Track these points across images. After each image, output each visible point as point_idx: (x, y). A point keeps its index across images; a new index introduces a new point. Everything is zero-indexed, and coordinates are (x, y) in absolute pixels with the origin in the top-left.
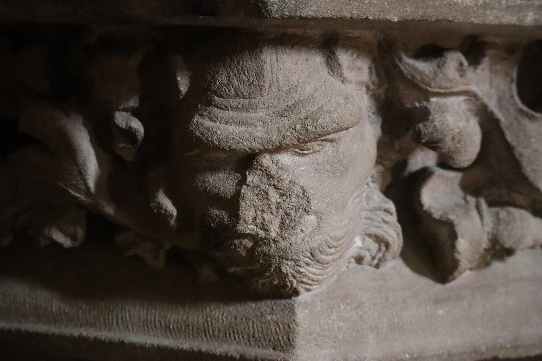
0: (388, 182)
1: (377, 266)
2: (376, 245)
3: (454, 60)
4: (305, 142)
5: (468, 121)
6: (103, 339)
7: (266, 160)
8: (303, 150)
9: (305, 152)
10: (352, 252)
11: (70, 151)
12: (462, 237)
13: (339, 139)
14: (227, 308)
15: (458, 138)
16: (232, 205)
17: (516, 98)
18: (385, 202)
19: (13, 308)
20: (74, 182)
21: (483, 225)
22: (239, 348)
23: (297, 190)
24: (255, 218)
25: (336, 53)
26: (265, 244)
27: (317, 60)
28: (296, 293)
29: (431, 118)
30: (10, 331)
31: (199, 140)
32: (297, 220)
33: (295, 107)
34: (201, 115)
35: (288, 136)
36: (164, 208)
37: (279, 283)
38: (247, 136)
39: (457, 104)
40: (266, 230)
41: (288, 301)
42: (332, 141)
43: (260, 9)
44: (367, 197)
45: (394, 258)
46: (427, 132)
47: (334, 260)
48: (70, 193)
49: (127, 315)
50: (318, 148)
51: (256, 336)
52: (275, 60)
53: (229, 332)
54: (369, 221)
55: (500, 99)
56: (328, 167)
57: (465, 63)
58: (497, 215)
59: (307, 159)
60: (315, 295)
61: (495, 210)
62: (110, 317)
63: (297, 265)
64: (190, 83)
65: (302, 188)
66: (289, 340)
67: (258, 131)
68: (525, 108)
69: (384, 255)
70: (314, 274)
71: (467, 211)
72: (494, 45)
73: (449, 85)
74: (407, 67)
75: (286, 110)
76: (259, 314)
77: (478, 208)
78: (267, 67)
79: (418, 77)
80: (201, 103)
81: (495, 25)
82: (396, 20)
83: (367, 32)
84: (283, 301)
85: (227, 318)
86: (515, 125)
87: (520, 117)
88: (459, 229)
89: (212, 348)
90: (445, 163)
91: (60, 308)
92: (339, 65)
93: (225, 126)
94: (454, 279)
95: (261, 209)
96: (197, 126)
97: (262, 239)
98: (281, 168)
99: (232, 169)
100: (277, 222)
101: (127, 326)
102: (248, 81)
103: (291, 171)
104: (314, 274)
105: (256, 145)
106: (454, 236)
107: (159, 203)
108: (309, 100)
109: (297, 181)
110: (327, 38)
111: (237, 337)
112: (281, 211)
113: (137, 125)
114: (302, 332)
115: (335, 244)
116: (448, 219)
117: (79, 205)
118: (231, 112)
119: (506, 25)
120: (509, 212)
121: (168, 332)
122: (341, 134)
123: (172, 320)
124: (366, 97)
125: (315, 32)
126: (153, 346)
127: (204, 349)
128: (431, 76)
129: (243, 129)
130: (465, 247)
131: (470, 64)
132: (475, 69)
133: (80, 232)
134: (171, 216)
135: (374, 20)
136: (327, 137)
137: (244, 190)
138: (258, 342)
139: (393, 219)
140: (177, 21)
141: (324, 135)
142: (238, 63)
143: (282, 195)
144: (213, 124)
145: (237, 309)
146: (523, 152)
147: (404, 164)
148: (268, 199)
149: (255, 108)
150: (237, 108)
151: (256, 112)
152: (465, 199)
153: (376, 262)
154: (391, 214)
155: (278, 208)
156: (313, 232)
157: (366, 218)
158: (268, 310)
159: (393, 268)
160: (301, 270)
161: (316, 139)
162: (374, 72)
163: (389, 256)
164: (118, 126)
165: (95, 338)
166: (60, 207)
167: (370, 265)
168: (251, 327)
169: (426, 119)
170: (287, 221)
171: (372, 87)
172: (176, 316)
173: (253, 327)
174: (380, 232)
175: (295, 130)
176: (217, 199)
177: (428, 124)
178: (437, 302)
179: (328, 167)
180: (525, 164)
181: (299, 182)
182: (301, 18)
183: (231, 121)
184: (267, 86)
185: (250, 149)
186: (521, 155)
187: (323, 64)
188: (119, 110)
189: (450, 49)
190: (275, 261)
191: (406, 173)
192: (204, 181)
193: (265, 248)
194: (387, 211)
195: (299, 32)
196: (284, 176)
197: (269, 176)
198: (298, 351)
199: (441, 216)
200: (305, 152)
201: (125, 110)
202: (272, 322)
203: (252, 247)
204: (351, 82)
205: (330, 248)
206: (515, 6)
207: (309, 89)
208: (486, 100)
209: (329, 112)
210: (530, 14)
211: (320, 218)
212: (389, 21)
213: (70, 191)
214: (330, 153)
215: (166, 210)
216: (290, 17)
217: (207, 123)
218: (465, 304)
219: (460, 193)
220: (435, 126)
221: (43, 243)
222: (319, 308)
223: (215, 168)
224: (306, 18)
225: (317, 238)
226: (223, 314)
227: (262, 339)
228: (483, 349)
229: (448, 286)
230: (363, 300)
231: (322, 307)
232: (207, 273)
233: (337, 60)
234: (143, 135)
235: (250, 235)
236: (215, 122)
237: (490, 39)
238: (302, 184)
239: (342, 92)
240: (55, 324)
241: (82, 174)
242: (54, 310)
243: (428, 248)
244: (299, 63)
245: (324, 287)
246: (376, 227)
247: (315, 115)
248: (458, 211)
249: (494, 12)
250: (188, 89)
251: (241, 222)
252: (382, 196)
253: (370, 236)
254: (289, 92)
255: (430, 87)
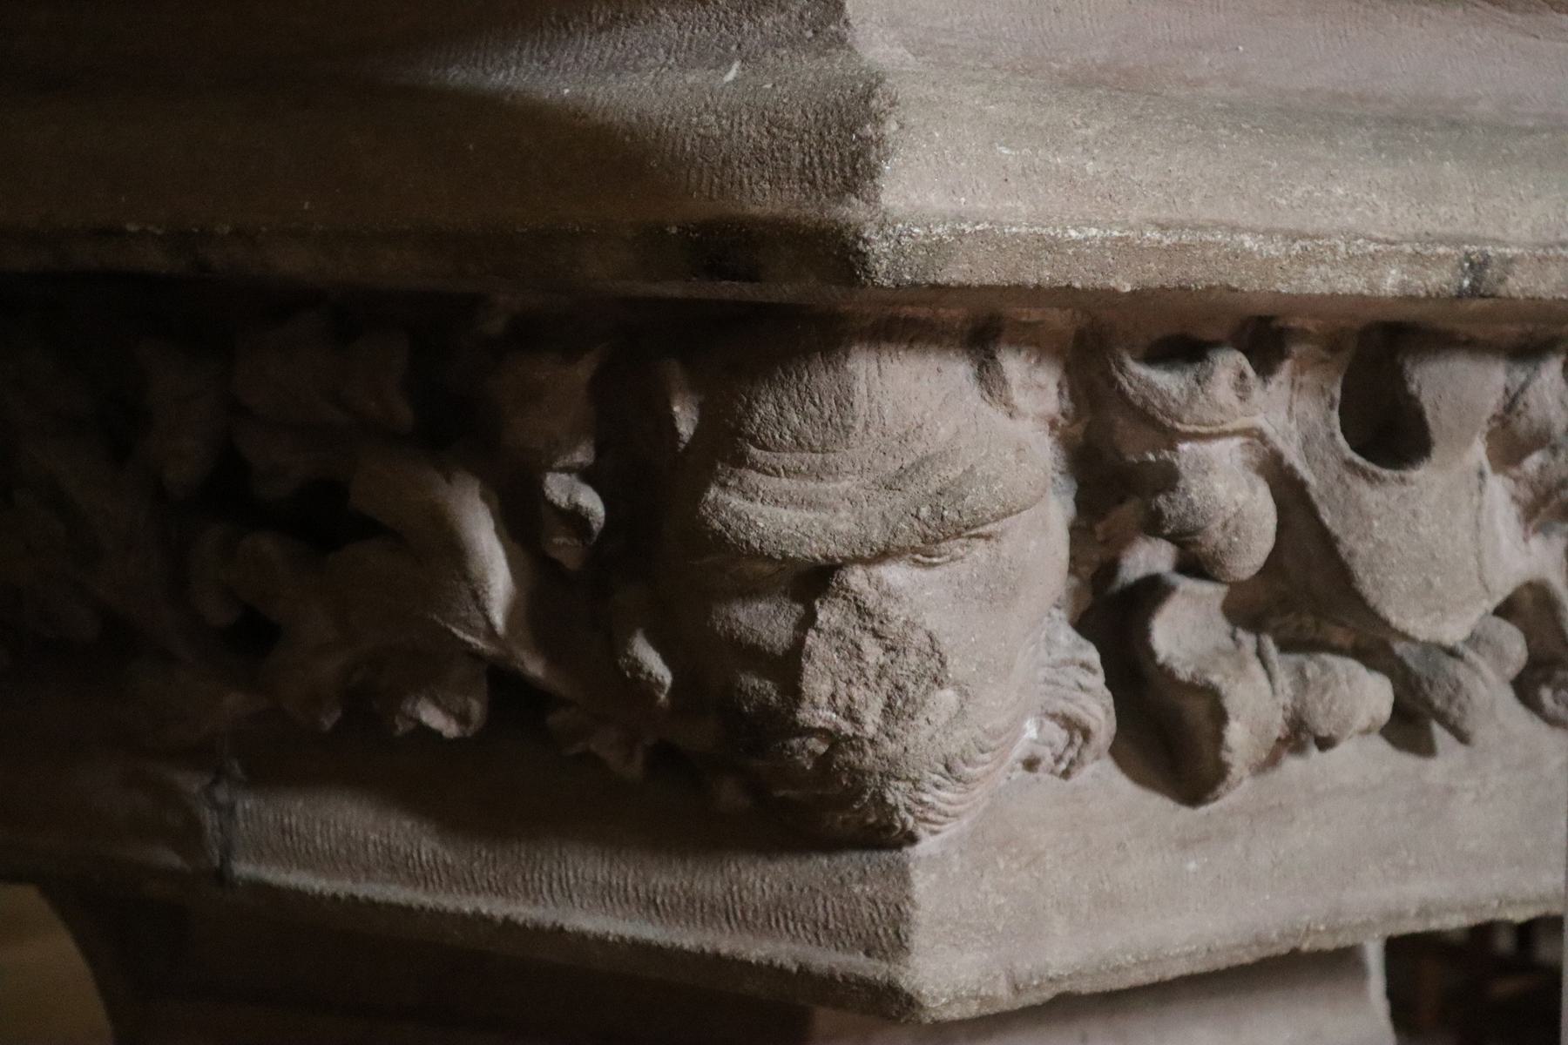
0: (1082, 608)
1: (1066, 774)
2: (1065, 734)
3: (1229, 364)
4: (937, 541)
5: (1253, 489)
6: (521, 920)
7: (856, 578)
8: (930, 556)
9: (935, 560)
10: (1019, 751)
11: (453, 552)
12: (1237, 718)
13: (1003, 533)
14: (771, 867)
15: (1235, 525)
16: (787, 667)
17: (1340, 438)
18: (1081, 647)
19: (343, 851)
20: (463, 614)
21: (1274, 693)
22: (797, 949)
23: (919, 638)
24: (833, 696)
25: (999, 357)
26: (853, 748)
27: (959, 371)
28: (912, 839)
29: (1181, 484)
30: (335, 897)
31: (720, 538)
32: (919, 700)
33: (917, 470)
34: (724, 486)
35: (902, 530)
36: (646, 668)
37: (878, 821)
38: (818, 530)
39: (1227, 454)
40: (851, 716)
41: (898, 855)
42: (988, 537)
43: (851, 267)
44: (1048, 639)
45: (1098, 758)
46: (1174, 513)
47: (988, 773)
48: (454, 636)
49: (571, 874)
50: (959, 551)
51: (831, 926)
52: (875, 373)
53: (776, 917)
54: (1051, 688)
55: (1307, 441)
56: (979, 589)
57: (1251, 373)
58: (1301, 670)
59: (936, 573)
60: (949, 841)
61: (1293, 659)
62: (536, 875)
63: (917, 789)
64: (701, 418)
65: (930, 636)
66: (898, 936)
67: (841, 521)
68: (1358, 459)
69: (1079, 753)
70: (949, 803)
71: (1241, 666)
72: (1303, 335)
73: (1218, 417)
74: (1135, 383)
75: (899, 477)
76: (836, 880)
77: (1260, 654)
78: (861, 387)
79: (1157, 402)
80: (723, 460)
81: (1322, 295)
82: (1128, 289)
83: (1056, 311)
84: (886, 856)
85: (772, 887)
86: (1338, 492)
87: (1348, 477)
88: (1231, 704)
89: (742, 948)
90: (1195, 564)
91: (435, 854)
92: (1004, 382)
93: (771, 510)
94: (1216, 799)
95: (845, 677)
96: (716, 510)
97: (847, 738)
98: (888, 594)
99: (785, 593)
100: (878, 704)
101: (570, 896)
102: (821, 416)
103: (906, 599)
104: (949, 803)
105: (836, 550)
106: (1220, 717)
107: (636, 660)
108: (943, 456)
109: (919, 621)
110: (977, 325)
111: (791, 926)
112: (886, 681)
113: (591, 501)
114: (924, 921)
115: (993, 744)
116: (1209, 683)
117: (475, 656)
118: (785, 481)
119: (1345, 295)
120: (1323, 665)
121: (653, 912)
122: (1006, 522)
123: (661, 888)
124: (1394, 620)
125: (954, 312)
126: (622, 938)
127: (724, 951)
128: (1183, 401)
129: (810, 515)
130: (1241, 738)
131: (1257, 371)
132: (1265, 382)
133: (476, 708)
134: (660, 685)
135: (1084, 290)
136: (981, 530)
137: (811, 639)
138: (835, 938)
139: (1097, 681)
140: (674, 289)
141: (975, 526)
142: (800, 378)
143: (888, 649)
144: (747, 504)
145: (791, 869)
146: (1356, 546)
147: (1110, 568)
148: (860, 658)
149: (835, 472)
150: (798, 472)
151: (836, 480)
152: (1233, 637)
153: (1063, 766)
154: (1095, 672)
155: (879, 677)
156: (950, 722)
157: (1047, 682)
158: (856, 874)
159: (1095, 776)
160: (926, 798)
161: (959, 535)
162: (1066, 392)
163: (1088, 755)
164: (551, 503)
165: (506, 919)
166: (434, 662)
167: (1052, 772)
168: (820, 909)
169: (1173, 489)
170: (899, 703)
171: (1062, 421)
172: (668, 879)
173: (825, 907)
174: (1072, 709)
175: (917, 517)
176: (754, 656)
177: (1177, 497)
178: (1184, 845)
179: (979, 589)
180: (1359, 570)
181: (924, 623)
182: (935, 286)
183: (785, 499)
184: (859, 427)
185: (825, 557)
186: (1351, 554)
187: (972, 380)
188: (555, 471)
189: (1216, 345)
190: (872, 782)
191: (1117, 586)
192: (728, 618)
193: (852, 756)
194: (1085, 666)
195: (923, 312)
196: (893, 611)
197: (863, 611)
198: (918, 960)
199: (1193, 675)
200: (935, 560)
201: (567, 470)
202: (863, 899)
203: (825, 754)
204: (1026, 416)
205: (982, 752)
206: (1363, 256)
207: (944, 433)
208: (1280, 444)
209: (987, 480)
210: (1393, 272)
211: (964, 694)
212: (1114, 292)
213: (455, 630)
214: (983, 560)
215: (650, 674)
216: (914, 285)
217: (736, 502)
218: (1238, 847)
219: (1223, 625)
220: (1191, 502)
221: (402, 728)
222: (956, 869)
223: (750, 591)
224: (946, 288)
225: (957, 734)
226: (762, 879)
227: (843, 934)
228: (1274, 935)
229: (1203, 810)
230: (1042, 847)
231: (962, 866)
232: (730, 794)
233: (1000, 373)
234: (602, 520)
235: (822, 730)
236: (752, 500)
237: (1295, 323)
238: (929, 627)
239: (999, 433)
240: (426, 886)
241: (478, 598)
242: (424, 857)
243: (1167, 739)
244: (925, 378)
245: (965, 822)
246: (1065, 698)
247: (959, 486)
248: (1225, 663)
249: (1322, 268)
250: (697, 431)
251: (806, 704)
252: (1074, 635)
253: (1053, 716)
254: (904, 439)
255: (1181, 422)
